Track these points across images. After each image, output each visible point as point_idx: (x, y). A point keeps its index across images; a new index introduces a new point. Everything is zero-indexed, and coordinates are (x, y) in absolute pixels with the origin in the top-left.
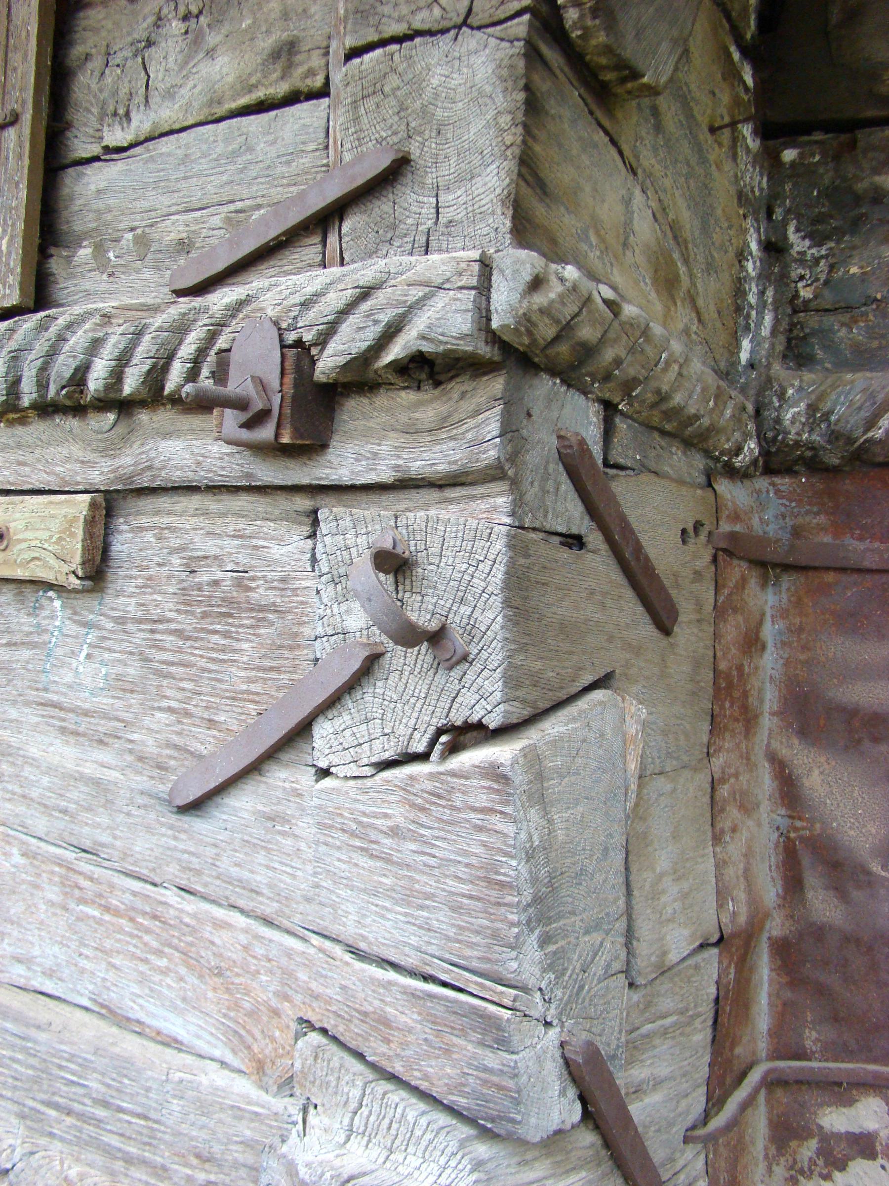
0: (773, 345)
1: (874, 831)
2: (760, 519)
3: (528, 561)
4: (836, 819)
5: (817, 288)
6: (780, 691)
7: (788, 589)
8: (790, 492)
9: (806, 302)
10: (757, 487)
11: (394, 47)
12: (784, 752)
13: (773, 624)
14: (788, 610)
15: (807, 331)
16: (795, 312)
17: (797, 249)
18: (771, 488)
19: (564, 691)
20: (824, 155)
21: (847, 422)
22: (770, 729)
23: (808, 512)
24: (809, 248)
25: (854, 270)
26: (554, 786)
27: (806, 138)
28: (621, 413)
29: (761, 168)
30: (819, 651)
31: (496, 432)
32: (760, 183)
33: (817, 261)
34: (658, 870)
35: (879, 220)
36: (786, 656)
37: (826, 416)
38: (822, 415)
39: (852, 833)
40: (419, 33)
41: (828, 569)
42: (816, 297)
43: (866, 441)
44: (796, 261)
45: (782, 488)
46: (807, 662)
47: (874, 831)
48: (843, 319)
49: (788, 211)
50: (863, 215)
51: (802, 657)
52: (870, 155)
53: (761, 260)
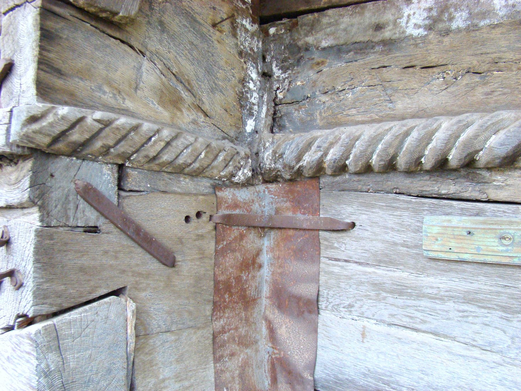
0: (266, 121)
1: (307, 357)
2: (260, 205)
3: (52, 242)
4: (290, 350)
5: (284, 93)
6: (270, 287)
7: (274, 238)
8: (275, 192)
9: (281, 100)
10: (257, 190)
11: (11, 13)
12: (271, 316)
13: (267, 255)
14: (273, 248)
15: (282, 113)
16: (276, 105)
17: (276, 75)
18: (266, 190)
19: (84, 298)
20: (286, 30)
21: (288, 159)
22: (265, 305)
23: (283, 201)
24: (281, 74)
25: (299, 83)
26: (66, 343)
27: (279, 22)
28: (128, 167)
29: (258, 38)
30: (286, 268)
31: (28, 186)
32: (257, 45)
33: (284, 80)
34: (161, 377)
35: (308, 58)
36: (272, 270)
37: (281, 156)
38: (279, 155)
39: (296, 357)
40: (18, 6)
41: (290, 229)
42: (284, 97)
43: (300, 167)
44: (276, 80)
45: (272, 190)
46: (281, 274)
47: (307, 357)
48: (296, 107)
49: (272, 57)
50: (302, 57)
51: (279, 271)
52: (304, 28)
53: (260, 82)
